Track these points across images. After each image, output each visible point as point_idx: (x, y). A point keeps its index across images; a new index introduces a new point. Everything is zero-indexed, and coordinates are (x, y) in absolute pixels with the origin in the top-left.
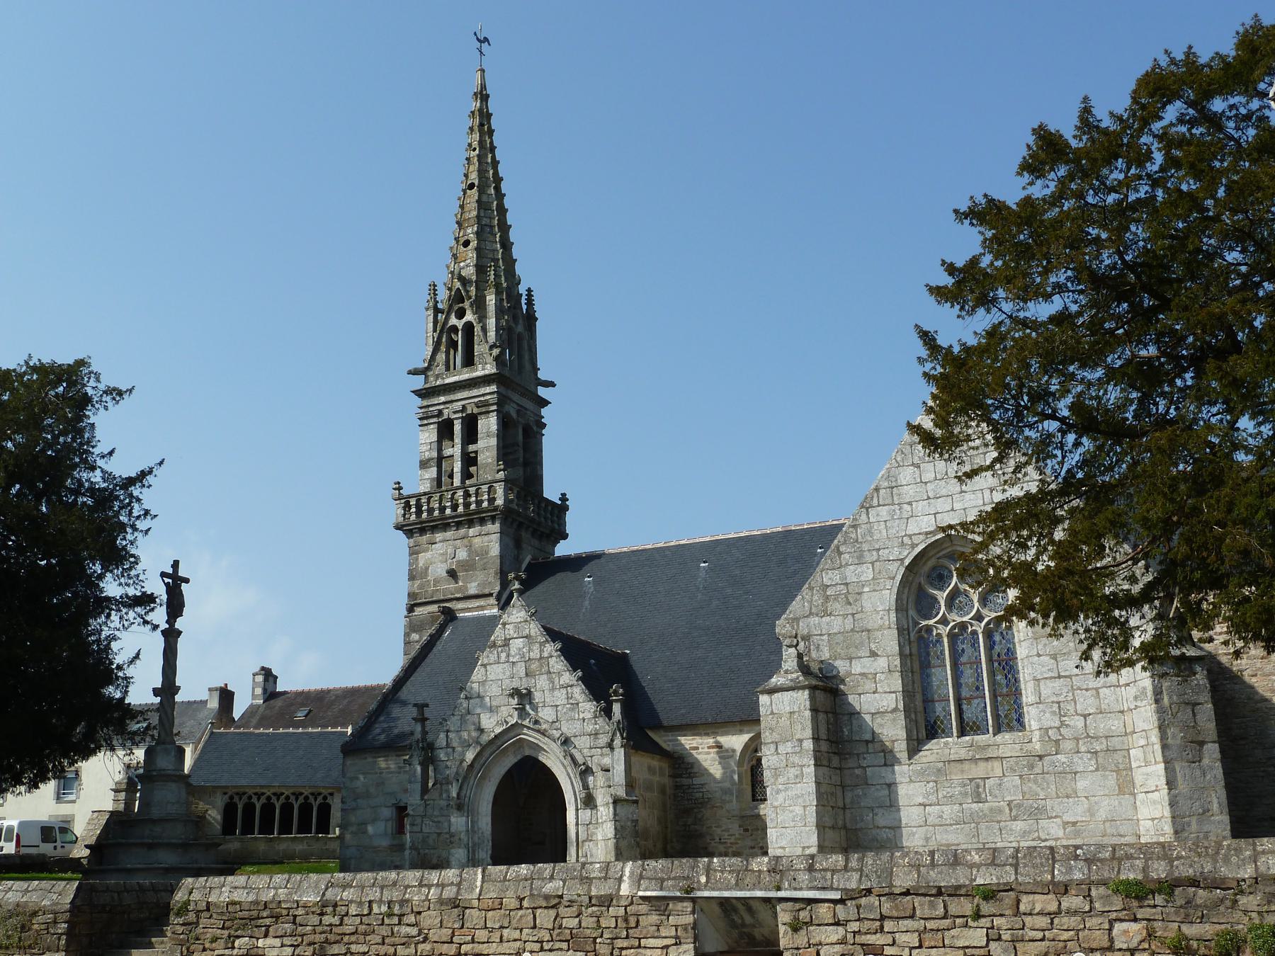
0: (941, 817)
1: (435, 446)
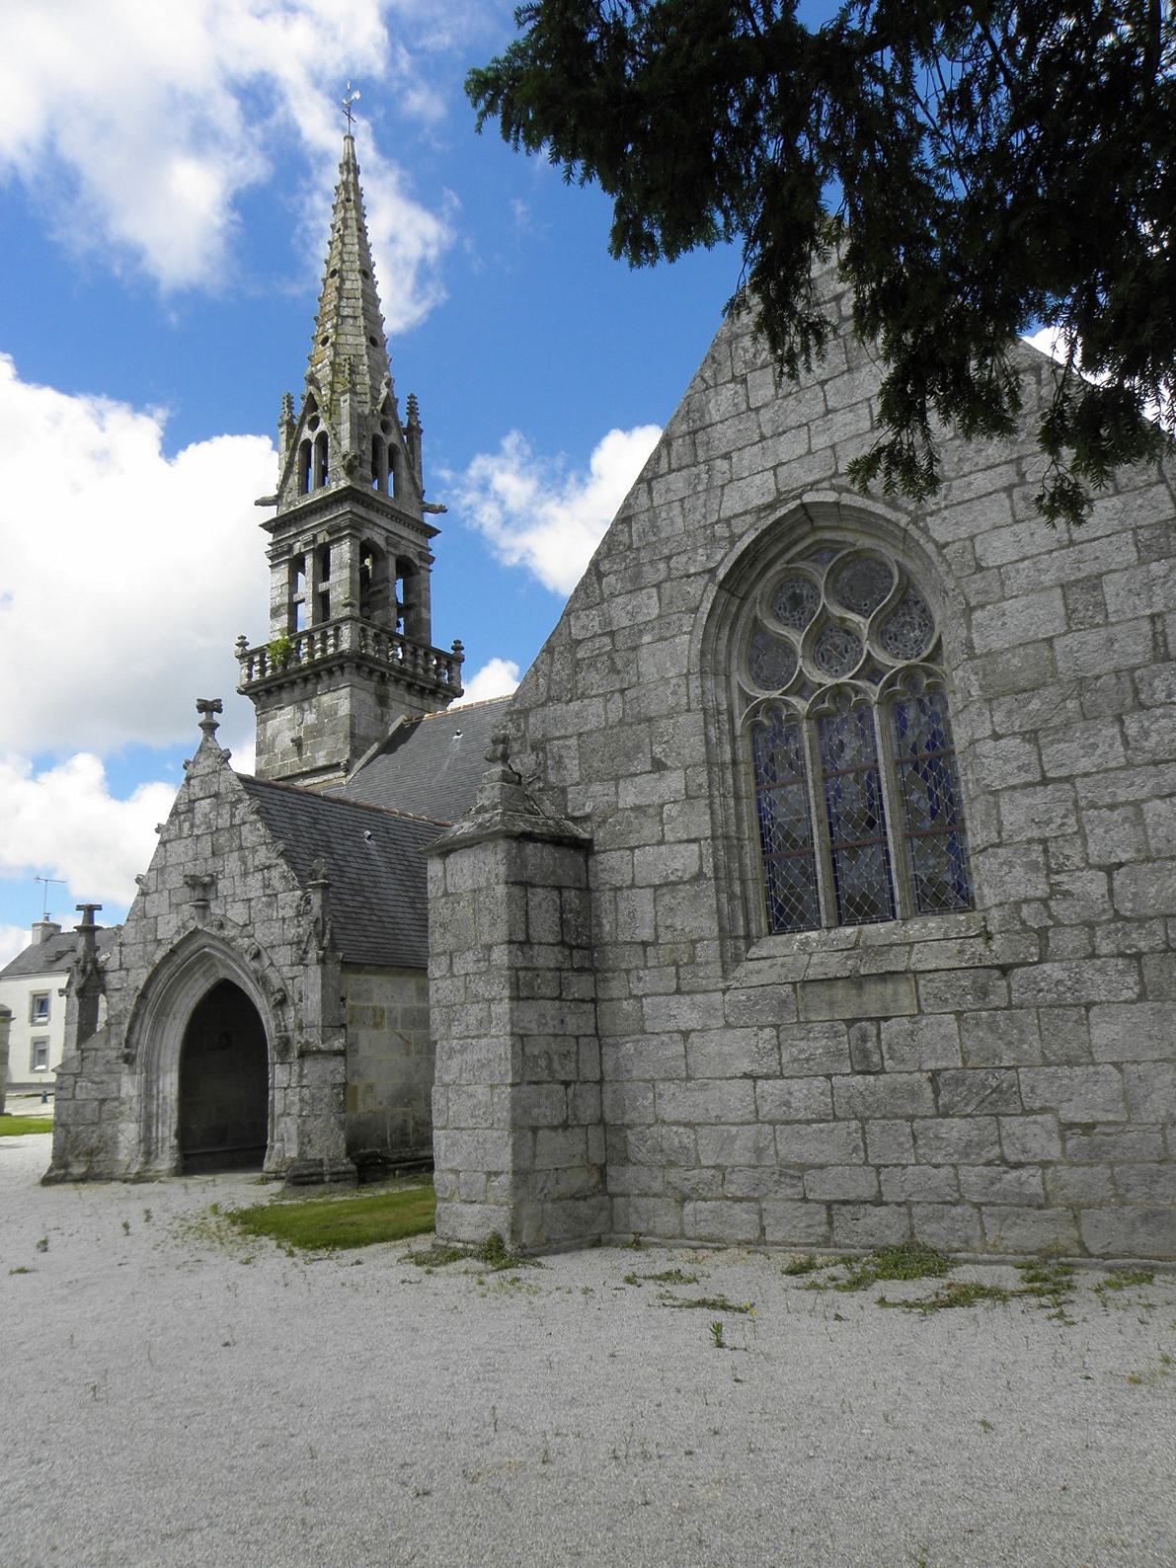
0: (787, 1104)
1: (286, 590)
